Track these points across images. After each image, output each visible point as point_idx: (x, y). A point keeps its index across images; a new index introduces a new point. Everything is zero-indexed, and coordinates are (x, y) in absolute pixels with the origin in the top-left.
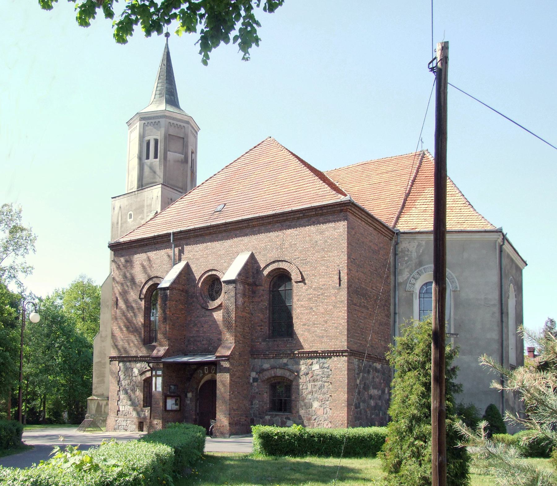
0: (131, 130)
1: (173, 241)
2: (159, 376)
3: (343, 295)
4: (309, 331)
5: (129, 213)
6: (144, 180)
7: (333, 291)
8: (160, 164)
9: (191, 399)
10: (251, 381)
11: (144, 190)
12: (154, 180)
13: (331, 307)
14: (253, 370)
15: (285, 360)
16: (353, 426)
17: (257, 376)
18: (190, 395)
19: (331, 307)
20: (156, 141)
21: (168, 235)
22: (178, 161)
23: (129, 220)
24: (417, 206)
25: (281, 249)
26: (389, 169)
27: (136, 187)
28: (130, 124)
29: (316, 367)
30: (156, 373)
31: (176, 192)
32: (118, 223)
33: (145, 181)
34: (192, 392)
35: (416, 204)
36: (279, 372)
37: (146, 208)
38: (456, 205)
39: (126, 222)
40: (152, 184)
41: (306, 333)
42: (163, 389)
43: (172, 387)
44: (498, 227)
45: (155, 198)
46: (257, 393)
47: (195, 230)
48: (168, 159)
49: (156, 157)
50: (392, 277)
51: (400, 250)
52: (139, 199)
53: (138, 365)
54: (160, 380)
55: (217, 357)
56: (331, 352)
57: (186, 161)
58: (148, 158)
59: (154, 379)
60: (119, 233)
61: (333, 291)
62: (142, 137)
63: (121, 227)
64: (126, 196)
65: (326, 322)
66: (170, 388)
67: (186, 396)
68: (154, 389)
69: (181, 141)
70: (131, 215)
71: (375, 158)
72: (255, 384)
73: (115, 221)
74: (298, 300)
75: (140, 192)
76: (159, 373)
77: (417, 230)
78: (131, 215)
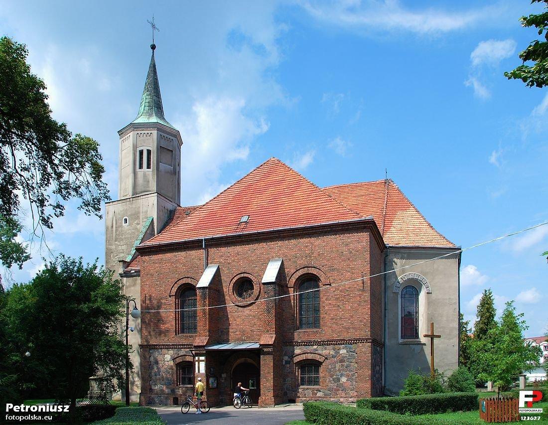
0: (123, 139)
1: (205, 246)
2: (199, 358)
3: (367, 296)
4: (337, 324)
5: (125, 218)
6: (138, 188)
7: (357, 293)
8: (153, 175)
9: (225, 379)
10: (284, 363)
11: (139, 198)
12: (148, 189)
13: (356, 305)
14: (285, 355)
15: (315, 347)
16: (376, 396)
17: (289, 359)
18: (224, 375)
19: (356, 305)
20: (149, 152)
21: (200, 241)
22: (168, 172)
23: (124, 224)
24: (394, 226)
25: (310, 257)
26: (362, 193)
27: (131, 194)
28: (122, 133)
29: (343, 351)
30: (199, 358)
31: (168, 201)
32: (112, 227)
33: (139, 189)
34: (227, 373)
35: (393, 224)
36: (310, 356)
37: (141, 214)
38: (422, 227)
39: (121, 226)
40: (146, 192)
41: (334, 326)
42: (206, 371)
43: (212, 369)
44: (457, 246)
45: (151, 204)
46: (289, 372)
47: (227, 237)
48: (160, 170)
49: (149, 167)
50: (383, 282)
51: (388, 260)
52: (134, 206)
53: (171, 352)
54: (202, 365)
55: (261, 345)
56: (355, 340)
57: (175, 173)
58: (141, 167)
59: (197, 363)
60: (114, 236)
61: (357, 293)
62: (135, 147)
63: (116, 230)
64: (120, 202)
65: (352, 317)
66: (210, 370)
67: (221, 376)
68: (197, 371)
69: (170, 153)
70: (126, 220)
71: (347, 183)
72: (288, 365)
73: (110, 225)
74: (326, 299)
75: (134, 199)
76: (202, 358)
77: (400, 245)
78: (126, 220)
